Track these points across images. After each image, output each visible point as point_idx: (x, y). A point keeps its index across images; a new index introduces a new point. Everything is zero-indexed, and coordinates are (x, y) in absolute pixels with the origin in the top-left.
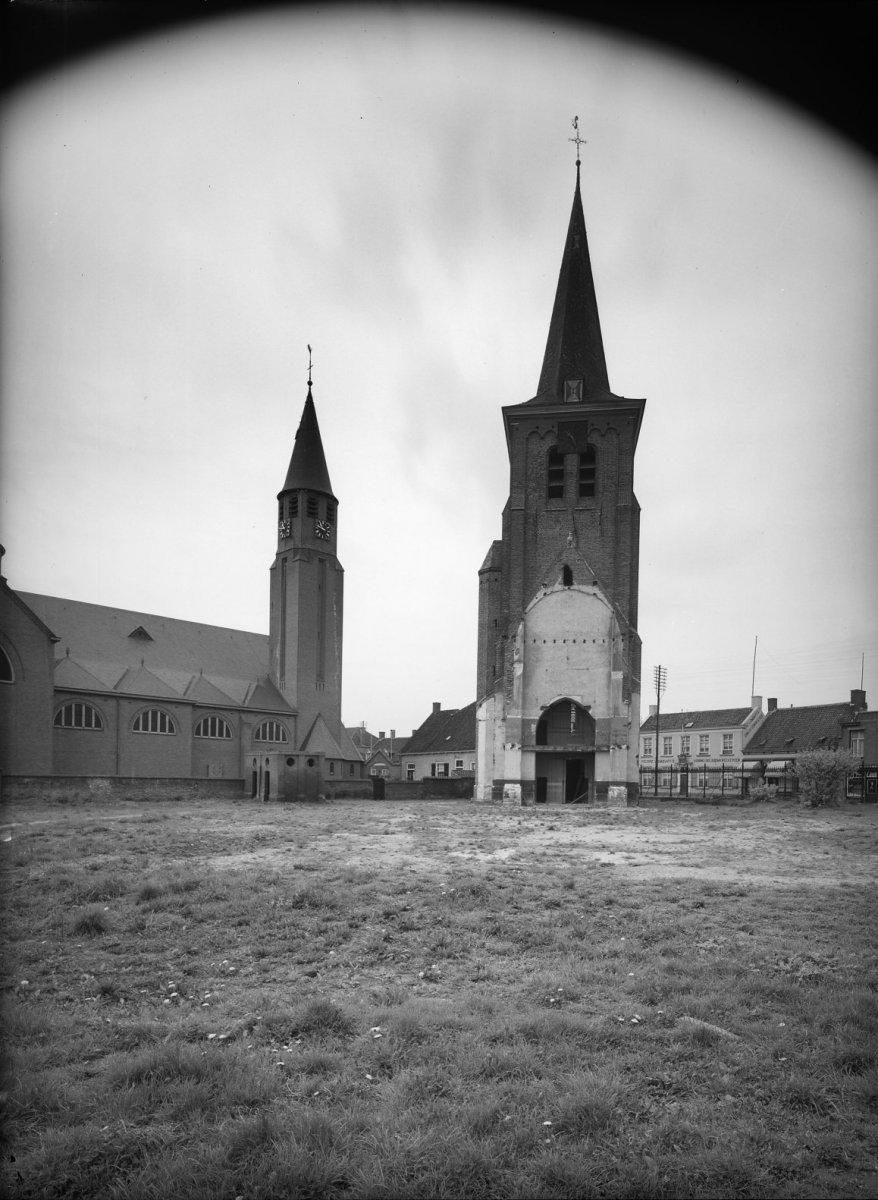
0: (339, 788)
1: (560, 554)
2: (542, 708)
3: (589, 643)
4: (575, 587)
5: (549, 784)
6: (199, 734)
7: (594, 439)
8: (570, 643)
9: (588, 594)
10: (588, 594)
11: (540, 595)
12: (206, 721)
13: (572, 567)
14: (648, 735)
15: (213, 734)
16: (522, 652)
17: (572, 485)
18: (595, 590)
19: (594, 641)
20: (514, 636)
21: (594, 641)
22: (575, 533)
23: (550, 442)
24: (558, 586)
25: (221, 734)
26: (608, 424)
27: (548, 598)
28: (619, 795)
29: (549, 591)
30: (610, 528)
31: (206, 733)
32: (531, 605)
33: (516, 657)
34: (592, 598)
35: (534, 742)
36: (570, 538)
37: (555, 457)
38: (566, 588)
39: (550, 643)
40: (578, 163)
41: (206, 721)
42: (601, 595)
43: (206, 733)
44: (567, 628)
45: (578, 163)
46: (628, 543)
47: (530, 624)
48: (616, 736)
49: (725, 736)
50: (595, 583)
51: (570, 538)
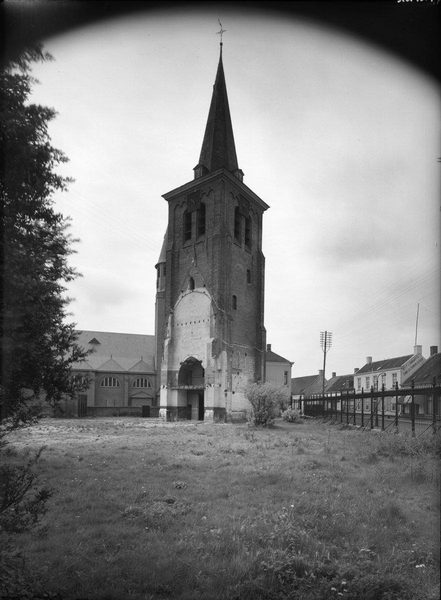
0: (122, 411)
1: (189, 272)
2: (181, 363)
3: (202, 322)
4: (195, 290)
5: (192, 409)
6: (142, 387)
7: (205, 200)
8: (193, 323)
9: (201, 293)
10: (201, 293)
11: (180, 296)
12: (106, 379)
13: (194, 279)
14: (394, 372)
15: (110, 385)
16: (170, 332)
17: (194, 230)
18: (204, 290)
19: (204, 321)
20: (167, 324)
21: (204, 321)
22: (196, 258)
23: (185, 208)
24: (188, 291)
25: (114, 385)
26: (210, 188)
27: (184, 299)
28: (210, 415)
29: (183, 295)
30: (210, 249)
31: (106, 385)
32: (176, 305)
33: (168, 335)
34: (203, 295)
35: (177, 384)
36: (193, 261)
37: (188, 215)
38: (191, 291)
39: (184, 325)
40: (221, 44)
41: (106, 379)
42: (207, 293)
43: (106, 385)
44: (191, 315)
45: (221, 44)
46: (218, 257)
47: (176, 315)
48: (209, 378)
49: (393, 375)
50: (204, 286)
51: (193, 261)
